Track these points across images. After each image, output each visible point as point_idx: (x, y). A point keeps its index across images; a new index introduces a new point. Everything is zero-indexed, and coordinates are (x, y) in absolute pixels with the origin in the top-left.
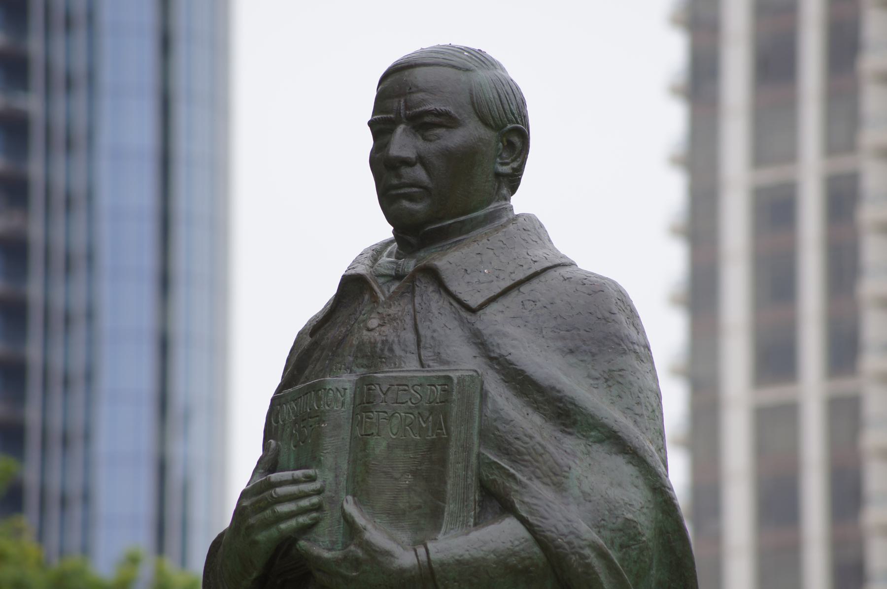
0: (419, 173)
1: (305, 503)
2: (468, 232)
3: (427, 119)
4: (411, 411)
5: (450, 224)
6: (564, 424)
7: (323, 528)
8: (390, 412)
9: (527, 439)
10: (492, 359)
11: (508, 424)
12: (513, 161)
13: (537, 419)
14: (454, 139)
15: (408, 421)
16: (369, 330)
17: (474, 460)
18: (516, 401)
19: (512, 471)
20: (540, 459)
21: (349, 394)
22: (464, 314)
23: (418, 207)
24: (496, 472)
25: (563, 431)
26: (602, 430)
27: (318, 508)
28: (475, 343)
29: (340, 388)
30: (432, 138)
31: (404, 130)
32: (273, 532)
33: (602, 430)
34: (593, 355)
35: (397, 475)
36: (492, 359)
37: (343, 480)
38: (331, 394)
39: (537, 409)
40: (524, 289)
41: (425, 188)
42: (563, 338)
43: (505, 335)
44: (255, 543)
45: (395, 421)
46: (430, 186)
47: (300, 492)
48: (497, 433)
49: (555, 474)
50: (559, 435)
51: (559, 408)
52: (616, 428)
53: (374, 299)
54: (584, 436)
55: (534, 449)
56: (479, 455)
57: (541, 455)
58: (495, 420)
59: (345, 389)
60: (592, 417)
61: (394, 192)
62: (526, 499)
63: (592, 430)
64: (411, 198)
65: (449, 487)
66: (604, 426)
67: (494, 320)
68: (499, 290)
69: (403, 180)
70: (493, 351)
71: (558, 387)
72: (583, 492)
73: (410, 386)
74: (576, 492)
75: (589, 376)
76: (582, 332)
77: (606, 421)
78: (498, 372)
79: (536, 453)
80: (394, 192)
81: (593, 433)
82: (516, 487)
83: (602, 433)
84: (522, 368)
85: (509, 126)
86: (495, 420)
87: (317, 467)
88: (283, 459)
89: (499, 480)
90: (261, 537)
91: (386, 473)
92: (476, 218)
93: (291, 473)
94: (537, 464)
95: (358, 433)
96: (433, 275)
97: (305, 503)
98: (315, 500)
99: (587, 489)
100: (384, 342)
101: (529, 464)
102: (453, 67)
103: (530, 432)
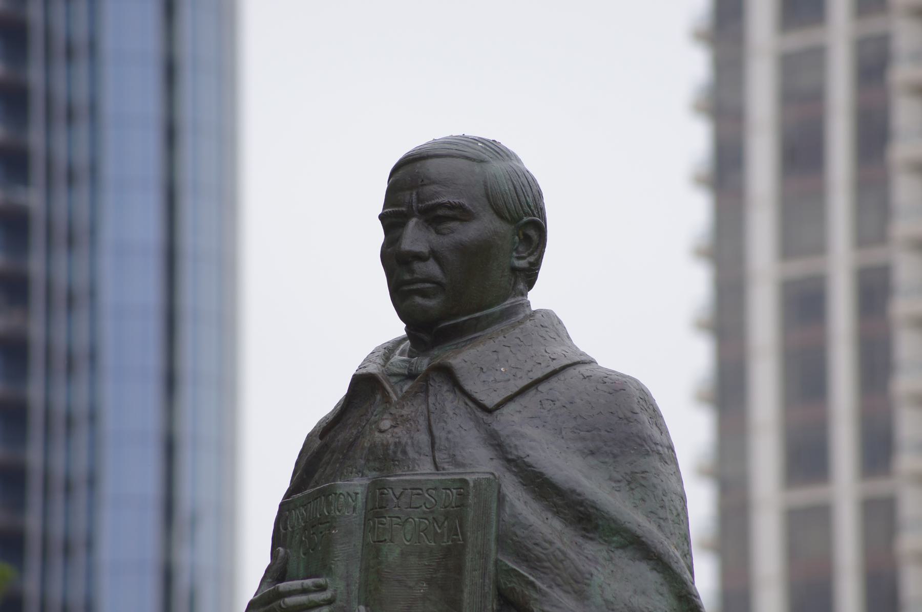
0: (432, 268)
2: (483, 329)
3: (440, 212)
4: (425, 516)
6: (585, 529)
9: (547, 545)
10: (509, 461)
11: (526, 529)
12: (530, 255)
13: (557, 524)
14: (469, 232)
15: (423, 527)
16: (381, 431)
17: (491, 567)
18: (535, 505)
19: (531, 578)
20: (560, 565)
22: (480, 414)
25: (584, 536)
28: (492, 445)
29: (351, 493)
31: (417, 223)
34: (615, 456)
36: (509, 461)
37: (354, 588)
38: (342, 499)
39: (557, 514)
40: (543, 388)
41: (439, 284)
42: (583, 439)
43: (523, 436)
45: (409, 527)
46: (444, 281)
50: (580, 540)
51: (580, 512)
53: (386, 399)
54: (606, 541)
56: (497, 562)
57: (561, 561)
58: (514, 525)
59: (357, 494)
60: (615, 521)
61: (406, 288)
63: (614, 535)
64: (424, 294)
66: (627, 531)
67: (512, 421)
68: (516, 389)
69: (415, 276)
71: (579, 490)
73: (424, 490)
74: (599, 600)
75: (611, 479)
76: (603, 433)
77: (628, 525)
78: (516, 474)
80: (406, 288)
81: (615, 539)
82: (535, 596)
84: (543, 470)
85: (525, 219)
86: (514, 525)
87: (328, 575)
89: (518, 589)
92: (493, 313)
94: (557, 571)
95: (370, 539)
96: (447, 373)
99: (610, 597)
102: (467, 158)
103: (549, 537)
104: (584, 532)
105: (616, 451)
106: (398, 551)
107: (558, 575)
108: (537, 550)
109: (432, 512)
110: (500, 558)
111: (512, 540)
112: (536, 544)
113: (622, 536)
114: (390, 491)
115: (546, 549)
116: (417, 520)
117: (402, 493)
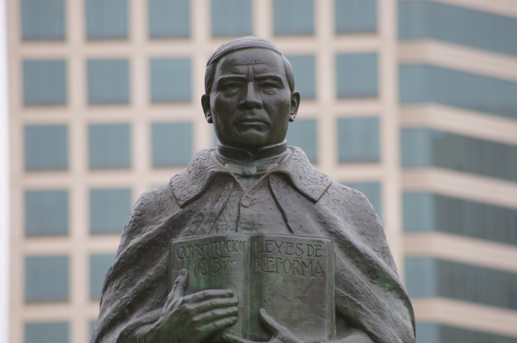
0: (262, 113)
1: (230, 310)
3: (268, 81)
4: (296, 260)
5: (274, 147)
6: (372, 277)
7: (239, 327)
8: (284, 259)
9: (361, 285)
10: (332, 233)
11: (349, 274)
16: (245, 207)
19: (359, 303)
20: (369, 297)
21: (247, 245)
23: (263, 134)
24: (348, 302)
25: (371, 281)
26: (392, 283)
27: (235, 314)
28: (320, 222)
29: (243, 242)
30: (271, 93)
32: (211, 325)
33: (392, 283)
34: (373, 237)
35: (291, 299)
36: (332, 233)
38: (237, 244)
39: (358, 266)
41: (267, 123)
43: (336, 219)
44: (198, 332)
46: (270, 122)
47: (228, 303)
48: (344, 278)
49: (379, 308)
51: (370, 267)
52: (399, 283)
53: (237, 185)
54: (382, 285)
55: (366, 291)
57: (369, 295)
58: (342, 271)
59: (245, 242)
62: (371, 321)
63: (386, 283)
64: (258, 128)
65: (327, 309)
67: (325, 206)
69: (255, 117)
70: (332, 228)
72: (394, 320)
73: (295, 244)
76: (365, 222)
79: (367, 293)
81: (387, 285)
82: (363, 313)
83: (392, 285)
84: (351, 240)
86: (342, 271)
88: (193, 281)
89: (351, 308)
90: (203, 328)
91: (283, 296)
93: (201, 292)
94: (368, 300)
96: (286, 179)
97: (230, 310)
98: (235, 309)
100: (259, 216)
101: (364, 300)
104: (371, 279)
105: (374, 234)
106: (281, 278)
107: (369, 302)
108: (357, 287)
109: (301, 258)
110: (338, 289)
111: (342, 279)
112: (356, 283)
113: (390, 284)
114: (274, 242)
115: (361, 287)
116: (292, 261)
117: (281, 245)
